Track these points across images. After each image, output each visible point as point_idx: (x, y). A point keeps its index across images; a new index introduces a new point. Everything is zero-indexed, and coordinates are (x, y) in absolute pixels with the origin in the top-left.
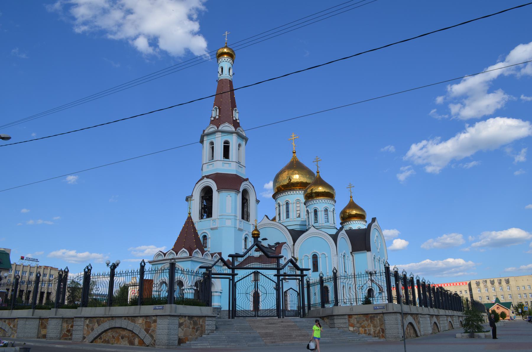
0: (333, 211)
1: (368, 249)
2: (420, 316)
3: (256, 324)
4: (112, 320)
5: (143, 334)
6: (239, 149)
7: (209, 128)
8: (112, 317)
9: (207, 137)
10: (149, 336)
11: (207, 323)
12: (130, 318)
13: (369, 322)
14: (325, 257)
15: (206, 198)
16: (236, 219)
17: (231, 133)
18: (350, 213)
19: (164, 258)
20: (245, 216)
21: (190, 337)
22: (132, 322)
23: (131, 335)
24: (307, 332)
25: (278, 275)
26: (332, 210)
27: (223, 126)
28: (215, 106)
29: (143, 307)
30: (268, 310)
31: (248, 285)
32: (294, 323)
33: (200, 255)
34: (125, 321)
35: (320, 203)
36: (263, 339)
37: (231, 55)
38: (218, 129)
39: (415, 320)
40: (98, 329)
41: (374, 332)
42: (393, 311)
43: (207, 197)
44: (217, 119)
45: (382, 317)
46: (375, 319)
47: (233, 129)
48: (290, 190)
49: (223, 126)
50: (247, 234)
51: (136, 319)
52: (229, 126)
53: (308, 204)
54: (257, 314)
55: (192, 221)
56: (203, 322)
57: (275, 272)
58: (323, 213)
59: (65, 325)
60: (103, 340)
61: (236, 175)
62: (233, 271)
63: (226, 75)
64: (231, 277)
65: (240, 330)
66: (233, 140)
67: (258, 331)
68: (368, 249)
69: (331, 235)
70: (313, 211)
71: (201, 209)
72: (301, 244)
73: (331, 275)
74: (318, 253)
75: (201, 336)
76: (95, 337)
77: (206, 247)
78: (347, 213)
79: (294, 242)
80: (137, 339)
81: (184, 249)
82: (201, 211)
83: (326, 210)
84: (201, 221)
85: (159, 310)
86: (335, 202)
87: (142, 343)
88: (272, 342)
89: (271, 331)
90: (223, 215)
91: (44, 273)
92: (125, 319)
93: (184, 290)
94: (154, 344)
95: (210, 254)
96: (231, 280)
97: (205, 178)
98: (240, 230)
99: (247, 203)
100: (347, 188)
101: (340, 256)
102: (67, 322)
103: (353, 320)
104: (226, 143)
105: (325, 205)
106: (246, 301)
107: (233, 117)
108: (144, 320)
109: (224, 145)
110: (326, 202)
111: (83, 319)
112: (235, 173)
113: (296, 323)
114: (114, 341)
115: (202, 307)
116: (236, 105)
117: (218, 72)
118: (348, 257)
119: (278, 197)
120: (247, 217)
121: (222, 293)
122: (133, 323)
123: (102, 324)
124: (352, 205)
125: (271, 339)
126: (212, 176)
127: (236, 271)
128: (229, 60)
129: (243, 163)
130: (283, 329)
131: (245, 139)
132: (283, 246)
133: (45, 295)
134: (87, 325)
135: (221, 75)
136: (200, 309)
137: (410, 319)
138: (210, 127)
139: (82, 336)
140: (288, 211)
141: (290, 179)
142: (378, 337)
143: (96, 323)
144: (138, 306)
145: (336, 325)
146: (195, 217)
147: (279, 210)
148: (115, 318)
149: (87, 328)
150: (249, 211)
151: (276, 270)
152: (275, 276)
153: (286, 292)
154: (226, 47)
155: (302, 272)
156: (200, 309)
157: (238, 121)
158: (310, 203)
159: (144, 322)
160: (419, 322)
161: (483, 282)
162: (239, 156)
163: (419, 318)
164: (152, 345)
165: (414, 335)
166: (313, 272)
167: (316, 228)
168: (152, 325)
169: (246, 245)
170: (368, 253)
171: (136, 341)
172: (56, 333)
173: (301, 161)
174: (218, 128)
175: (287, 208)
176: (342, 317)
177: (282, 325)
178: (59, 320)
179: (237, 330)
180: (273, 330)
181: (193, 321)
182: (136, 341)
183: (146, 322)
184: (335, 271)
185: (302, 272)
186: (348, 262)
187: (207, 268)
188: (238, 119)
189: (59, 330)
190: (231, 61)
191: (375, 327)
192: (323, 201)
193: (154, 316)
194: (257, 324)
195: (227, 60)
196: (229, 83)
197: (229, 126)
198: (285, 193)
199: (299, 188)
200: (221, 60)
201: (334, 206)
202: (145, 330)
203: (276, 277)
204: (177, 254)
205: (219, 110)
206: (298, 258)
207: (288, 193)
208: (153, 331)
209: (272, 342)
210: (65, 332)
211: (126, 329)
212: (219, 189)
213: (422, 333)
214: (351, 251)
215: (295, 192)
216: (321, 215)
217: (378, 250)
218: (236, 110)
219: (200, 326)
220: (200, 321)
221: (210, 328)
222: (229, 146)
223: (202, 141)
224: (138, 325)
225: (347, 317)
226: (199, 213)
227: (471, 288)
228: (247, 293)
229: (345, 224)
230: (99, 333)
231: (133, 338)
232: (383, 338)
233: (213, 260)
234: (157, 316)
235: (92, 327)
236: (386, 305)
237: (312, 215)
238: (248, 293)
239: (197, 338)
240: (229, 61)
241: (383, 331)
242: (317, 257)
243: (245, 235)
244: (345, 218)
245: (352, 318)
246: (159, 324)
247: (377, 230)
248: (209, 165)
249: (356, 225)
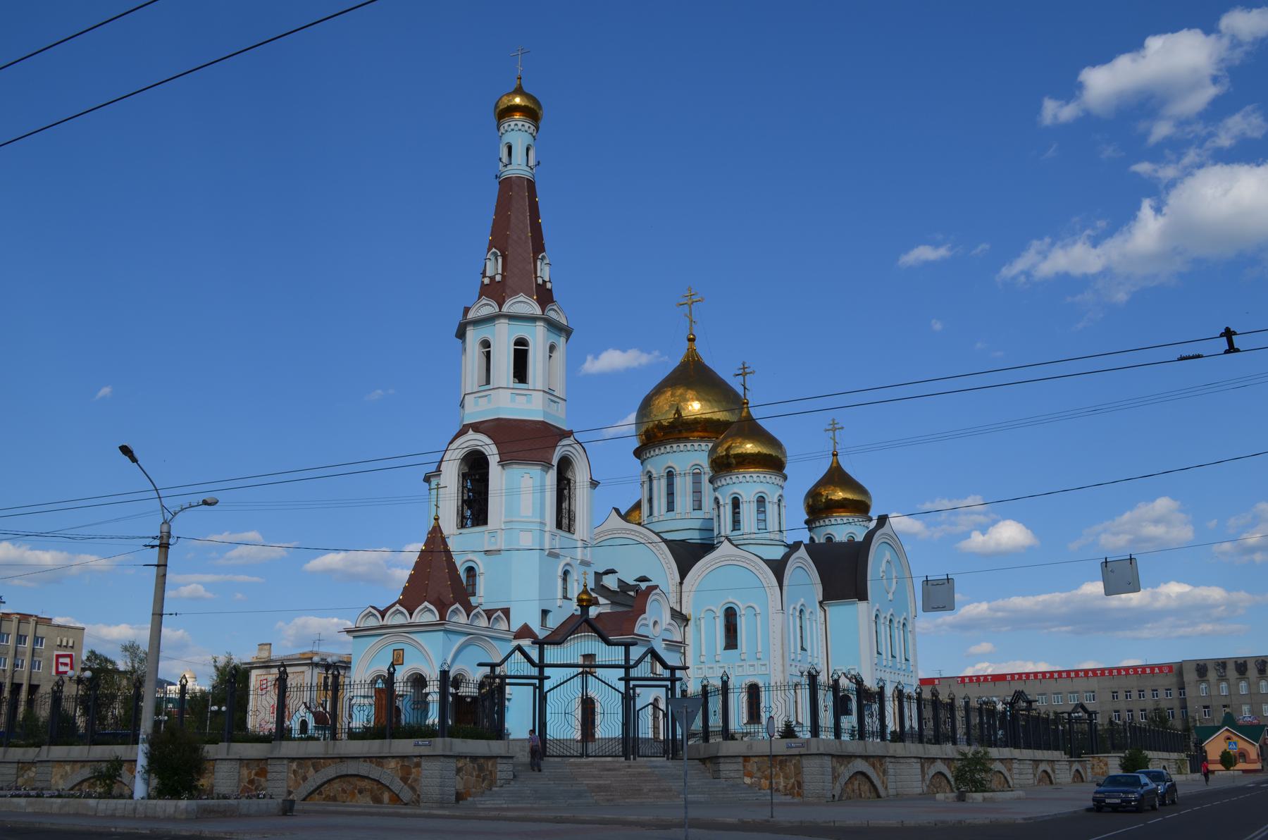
0: (779, 500)
1: (863, 596)
2: (888, 759)
3: (582, 770)
4: (341, 762)
5: (397, 785)
6: (550, 357)
7: (478, 306)
8: (341, 758)
9: (474, 326)
10: (408, 789)
11: (499, 767)
12: (374, 760)
13: (778, 769)
14: (755, 615)
15: (473, 477)
16: (542, 531)
17: (532, 319)
18: (829, 497)
19: (381, 623)
20: (565, 521)
21: (474, 790)
22: (378, 766)
23: (375, 787)
24: (670, 784)
25: (627, 679)
26: (776, 500)
27: (512, 302)
28: (494, 250)
29: (396, 741)
30: (612, 739)
31: (568, 698)
32: (649, 770)
33: (462, 618)
34: (365, 764)
35: (747, 482)
36: (593, 794)
37: (532, 114)
38: (500, 311)
39: (874, 768)
40: (315, 779)
41: (785, 786)
42: (818, 752)
43: (475, 475)
44: (499, 282)
45: (799, 761)
46: (788, 764)
47: (537, 310)
48: (678, 440)
49: (512, 302)
50: (568, 564)
51: (385, 761)
52: (529, 302)
53: (719, 484)
54: (586, 752)
55: (441, 536)
56: (492, 765)
57: (621, 672)
58: (754, 506)
59: (245, 772)
60: (324, 796)
61: (543, 422)
62: (541, 672)
63: (518, 167)
64: (536, 681)
65: (554, 780)
66: (537, 337)
67: (585, 782)
68: (863, 596)
69: (768, 562)
70: (729, 501)
71: (460, 503)
72: (698, 581)
73: (719, 683)
74: (736, 605)
75: (491, 790)
76: (309, 792)
77: (475, 595)
78: (822, 495)
79: (683, 576)
80: (387, 793)
81: (426, 603)
82: (460, 509)
83: (761, 499)
84: (460, 533)
85: (423, 747)
86: (785, 478)
87: (396, 799)
88: (608, 800)
89: (607, 782)
90: (512, 521)
91: (37, 635)
92: (365, 761)
93: (427, 694)
94: (418, 802)
95: (484, 611)
96: (537, 688)
97: (471, 432)
98: (553, 555)
99: (570, 489)
100: (826, 430)
101: (791, 612)
102: (248, 766)
103: (752, 766)
104: (521, 342)
105: (760, 488)
106: (565, 728)
107: (536, 277)
108: (398, 763)
109: (515, 349)
110: (762, 479)
111: (285, 762)
112: (542, 419)
113: (653, 769)
114: (345, 798)
115: (490, 742)
116: (543, 245)
117: (500, 159)
118: (811, 612)
119: (648, 455)
120: (569, 522)
121: (511, 702)
122: (380, 768)
123: (323, 770)
124: (836, 476)
125: (606, 795)
126: (486, 424)
127: (547, 671)
128: (527, 125)
129: (559, 392)
130: (629, 779)
131: (565, 331)
132: (640, 618)
133: (23, 695)
134: (294, 771)
135: (506, 166)
136: (488, 745)
137: (1043, 767)
138: (481, 304)
139: (285, 790)
140: (670, 494)
141: (678, 412)
142: (791, 795)
143: (986, 753)
144: (387, 741)
145: (722, 774)
146: (449, 524)
147: (651, 490)
148: (346, 760)
149: (295, 776)
150: (573, 509)
151: (623, 669)
152: (620, 679)
153: (638, 711)
154: (519, 91)
155: (673, 673)
156: (488, 745)
157: (549, 286)
158: (723, 480)
159: (399, 766)
160: (885, 772)
161: (1218, 668)
162: (548, 374)
163: (888, 763)
164: (413, 802)
165: (874, 794)
166: (725, 649)
167: (734, 542)
168: (413, 770)
169: (566, 589)
170: (862, 605)
171: (386, 797)
172: (230, 786)
173: (708, 361)
174: (500, 307)
175: (670, 485)
176: (734, 760)
177: (628, 772)
178: (234, 763)
179: (549, 780)
180: (611, 781)
181: (478, 765)
182: (386, 797)
183: (402, 766)
184: (725, 678)
185: (673, 673)
186: (811, 626)
187: (493, 666)
188: (550, 281)
189: (235, 781)
190: (532, 127)
191: (786, 778)
192: (755, 479)
193: (416, 756)
194: (584, 770)
195: (523, 125)
196: (526, 189)
197: (529, 302)
198: (665, 448)
199: (701, 434)
200: (506, 125)
201: (783, 488)
202: (401, 779)
203: (623, 682)
204: (411, 615)
205: (503, 259)
206: (690, 615)
207: (672, 447)
208: (416, 780)
209: (608, 800)
210: (246, 784)
211: (367, 778)
212: (503, 462)
213: (892, 792)
214: (821, 599)
215: (689, 445)
216: (748, 513)
217: (890, 596)
218: (543, 259)
219: (488, 773)
220: (488, 765)
221: (504, 775)
222: (526, 352)
223: (461, 334)
224: (389, 771)
225: (741, 760)
226: (458, 514)
227: (1183, 683)
229: (815, 523)
230: (318, 784)
231: (380, 791)
232: (799, 797)
233: (490, 626)
234: (421, 756)
235: (303, 774)
236: (807, 742)
237: (727, 512)
238: (570, 711)
239: (483, 793)
240: (527, 128)
241: (800, 785)
242: (736, 614)
243: (563, 568)
244: (818, 509)
245: (749, 762)
246: (426, 770)
247: (893, 547)
248: (480, 397)
249: (843, 529)
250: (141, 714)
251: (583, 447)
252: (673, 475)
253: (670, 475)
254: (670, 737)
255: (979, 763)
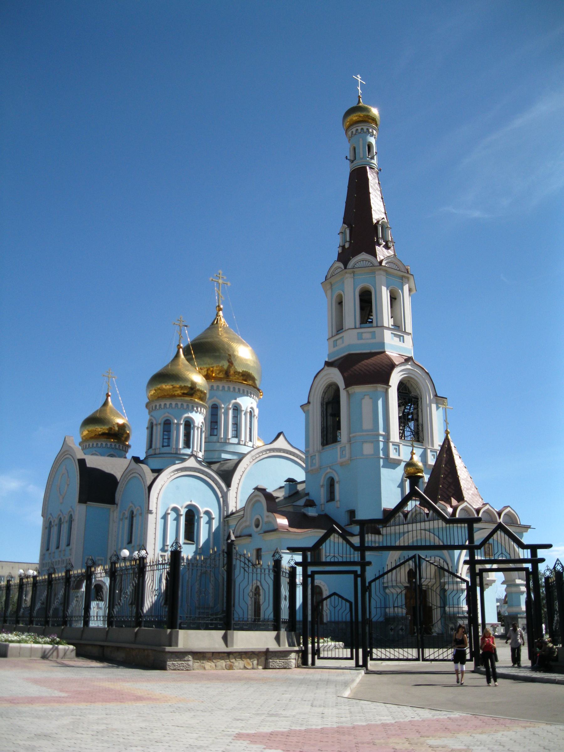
64: (358, 569)
155: (534, 554)
164: (180, 701)
185: (534, 554)
226: (422, 425)
228: (396, 605)
250: (249, 648)
251: (347, 330)
252: (170, 424)
253: (167, 424)
254: (309, 618)
255: (453, 629)
